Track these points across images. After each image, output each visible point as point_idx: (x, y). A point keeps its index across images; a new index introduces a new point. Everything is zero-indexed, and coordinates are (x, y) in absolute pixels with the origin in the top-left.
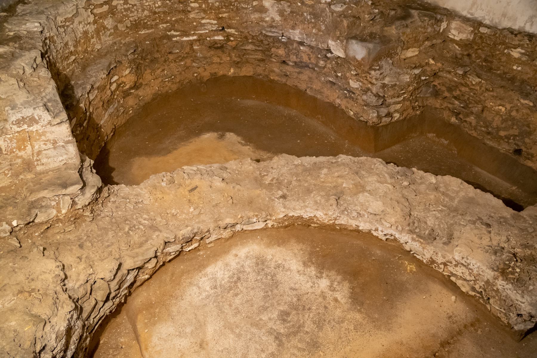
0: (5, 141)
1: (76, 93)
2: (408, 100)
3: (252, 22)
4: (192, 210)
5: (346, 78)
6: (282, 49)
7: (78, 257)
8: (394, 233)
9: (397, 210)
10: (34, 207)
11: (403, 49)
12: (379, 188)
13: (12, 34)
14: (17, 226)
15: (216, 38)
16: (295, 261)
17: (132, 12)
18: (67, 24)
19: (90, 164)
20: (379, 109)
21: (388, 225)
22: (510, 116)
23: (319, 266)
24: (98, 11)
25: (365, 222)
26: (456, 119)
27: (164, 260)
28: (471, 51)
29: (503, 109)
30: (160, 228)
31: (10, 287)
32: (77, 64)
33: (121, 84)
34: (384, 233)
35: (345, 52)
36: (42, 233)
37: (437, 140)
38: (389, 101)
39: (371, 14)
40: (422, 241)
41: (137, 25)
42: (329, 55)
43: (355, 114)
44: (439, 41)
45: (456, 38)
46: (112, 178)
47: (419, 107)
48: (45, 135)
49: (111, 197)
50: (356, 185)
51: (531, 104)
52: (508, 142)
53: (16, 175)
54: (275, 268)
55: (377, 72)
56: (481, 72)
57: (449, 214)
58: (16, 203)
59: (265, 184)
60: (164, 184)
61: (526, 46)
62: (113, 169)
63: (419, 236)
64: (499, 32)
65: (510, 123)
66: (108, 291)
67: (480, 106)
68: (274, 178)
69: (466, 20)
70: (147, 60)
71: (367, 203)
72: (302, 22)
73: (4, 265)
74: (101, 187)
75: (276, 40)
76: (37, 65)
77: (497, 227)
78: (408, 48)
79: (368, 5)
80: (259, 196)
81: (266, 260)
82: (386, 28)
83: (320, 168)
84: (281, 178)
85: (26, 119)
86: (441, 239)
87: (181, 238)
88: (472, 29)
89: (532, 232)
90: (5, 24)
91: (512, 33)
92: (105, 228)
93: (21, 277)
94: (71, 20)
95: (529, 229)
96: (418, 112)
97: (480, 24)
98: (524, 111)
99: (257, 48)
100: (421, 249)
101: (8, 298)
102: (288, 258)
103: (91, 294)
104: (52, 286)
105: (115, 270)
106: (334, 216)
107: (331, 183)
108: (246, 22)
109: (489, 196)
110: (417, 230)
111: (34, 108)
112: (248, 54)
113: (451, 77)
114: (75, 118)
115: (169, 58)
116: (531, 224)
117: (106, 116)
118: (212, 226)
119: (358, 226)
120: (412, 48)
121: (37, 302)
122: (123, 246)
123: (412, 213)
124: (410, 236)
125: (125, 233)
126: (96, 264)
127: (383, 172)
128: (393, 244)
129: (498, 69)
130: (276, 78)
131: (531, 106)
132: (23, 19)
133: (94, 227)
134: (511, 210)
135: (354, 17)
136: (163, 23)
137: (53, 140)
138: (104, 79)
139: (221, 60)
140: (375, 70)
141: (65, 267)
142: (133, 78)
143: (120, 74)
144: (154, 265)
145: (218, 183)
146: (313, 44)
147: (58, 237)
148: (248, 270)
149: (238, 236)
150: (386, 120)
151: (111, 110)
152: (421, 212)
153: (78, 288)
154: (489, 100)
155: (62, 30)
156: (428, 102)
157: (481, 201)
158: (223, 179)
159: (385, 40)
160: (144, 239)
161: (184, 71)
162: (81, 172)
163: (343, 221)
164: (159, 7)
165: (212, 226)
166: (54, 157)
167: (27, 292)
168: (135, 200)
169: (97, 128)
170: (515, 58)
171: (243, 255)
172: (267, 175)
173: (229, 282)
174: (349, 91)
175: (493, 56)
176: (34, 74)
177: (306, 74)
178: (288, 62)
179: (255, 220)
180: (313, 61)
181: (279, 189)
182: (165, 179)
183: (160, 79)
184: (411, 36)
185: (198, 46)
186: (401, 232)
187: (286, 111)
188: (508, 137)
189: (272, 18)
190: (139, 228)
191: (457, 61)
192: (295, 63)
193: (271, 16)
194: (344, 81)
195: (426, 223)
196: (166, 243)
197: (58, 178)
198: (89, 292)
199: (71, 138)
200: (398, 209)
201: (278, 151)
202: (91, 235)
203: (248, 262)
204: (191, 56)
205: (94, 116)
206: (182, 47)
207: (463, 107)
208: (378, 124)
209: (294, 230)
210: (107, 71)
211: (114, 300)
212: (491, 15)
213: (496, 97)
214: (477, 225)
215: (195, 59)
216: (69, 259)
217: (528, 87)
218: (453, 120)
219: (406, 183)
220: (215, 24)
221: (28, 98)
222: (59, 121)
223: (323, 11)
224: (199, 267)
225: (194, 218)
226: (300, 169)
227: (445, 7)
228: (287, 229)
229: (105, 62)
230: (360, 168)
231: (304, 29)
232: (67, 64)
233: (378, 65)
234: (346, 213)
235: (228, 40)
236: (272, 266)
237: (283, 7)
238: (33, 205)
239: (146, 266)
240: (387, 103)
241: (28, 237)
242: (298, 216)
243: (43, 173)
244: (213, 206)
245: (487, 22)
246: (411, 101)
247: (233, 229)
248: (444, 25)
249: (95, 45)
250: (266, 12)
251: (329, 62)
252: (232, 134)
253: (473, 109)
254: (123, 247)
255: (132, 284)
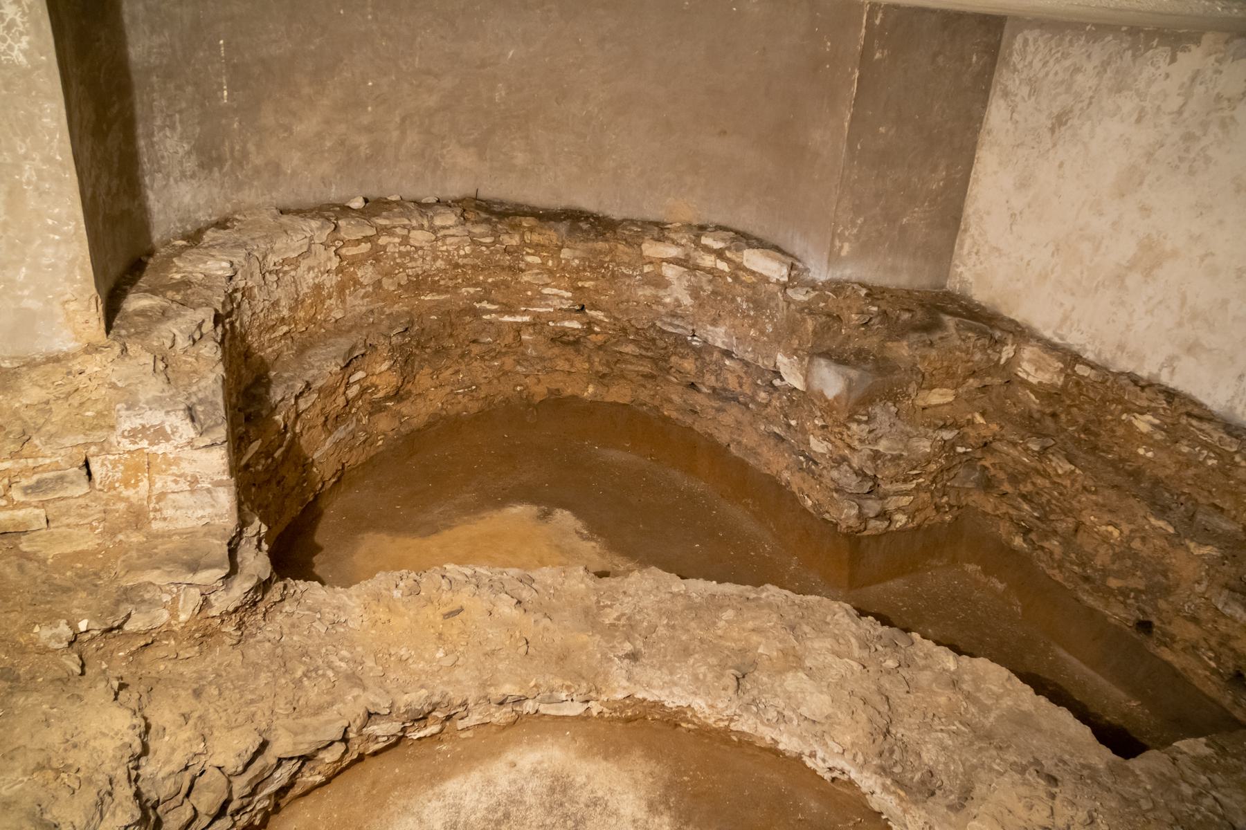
0: (103, 465)
1: (272, 393)
2: (927, 489)
3: (638, 303)
4: (440, 654)
5: (804, 432)
6: (691, 360)
7: (183, 715)
8: (847, 768)
9: (858, 719)
10: (127, 600)
11: (920, 388)
12: (831, 667)
13: (178, 276)
14: (87, 631)
15: (567, 324)
16: (631, 797)
17: (412, 259)
18: (286, 268)
19: (259, 533)
20: (862, 502)
21: (838, 749)
22: (1130, 548)
23: (680, 817)
24: (348, 251)
25: (792, 734)
26: (1025, 540)
27: (362, 749)
28: (1059, 409)
29: (1116, 533)
30: (366, 682)
31: (25, 754)
32: (289, 342)
33: (368, 388)
34: (827, 765)
35: (806, 380)
36: (132, 654)
37: (983, 579)
38: (886, 487)
39: (863, 313)
40: (902, 794)
41: (418, 284)
42: (777, 382)
43: (814, 505)
44: (998, 381)
45: (1031, 379)
46: (313, 565)
47: (951, 507)
48: (178, 465)
49: (286, 603)
50: (785, 653)
51: (1171, 530)
52: (1124, 603)
53: (112, 532)
54: (587, 806)
55: (863, 426)
56: (1076, 452)
57: (971, 744)
58: (96, 586)
59: (602, 623)
60: (397, 594)
61: (1161, 411)
62: (319, 549)
63: (898, 783)
64: (1111, 378)
65: (1129, 563)
66: (225, 796)
67: (1070, 520)
68: (623, 615)
69: (1050, 347)
70: (428, 350)
71: (799, 695)
72: (732, 313)
73: (34, 705)
74: (270, 579)
75: (680, 341)
76: (202, 336)
77: (1071, 786)
78: (931, 388)
79: (859, 296)
80: (583, 647)
81: (571, 785)
82: (889, 344)
83: (721, 608)
84: (638, 617)
85: (149, 429)
86: (947, 797)
87: (403, 710)
88: (1061, 365)
89: (1148, 811)
90: (175, 260)
91: (1136, 383)
92: (255, 665)
93: (54, 737)
94: (295, 262)
95: (1142, 802)
96: (948, 518)
97: (1077, 358)
98: (1157, 542)
99: (644, 353)
100: (898, 811)
101: (13, 776)
102: (619, 789)
103: (188, 795)
104: (107, 767)
105: (249, 754)
106: (728, 712)
107: (735, 641)
108: (628, 301)
109: (1064, 715)
110: (897, 769)
111: (167, 413)
112: (625, 362)
113: (1017, 453)
114: (260, 441)
115: (470, 351)
116: (1149, 792)
117: (328, 444)
118: (472, 696)
119: (777, 742)
120: (942, 386)
121: (65, 794)
122: (282, 706)
123: (893, 731)
124: (880, 781)
125: (294, 681)
126: (216, 734)
127: (847, 633)
128: (846, 791)
129: (1109, 450)
130: (674, 415)
131: (1170, 535)
132: (207, 254)
133: (236, 657)
134: (1107, 753)
135: (829, 315)
136: (469, 286)
137: (192, 476)
138: (336, 374)
139: (572, 366)
140: (859, 422)
141: (152, 731)
142: (394, 380)
143: (370, 370)
144: (337, 757)
145: (506, 608)
146: (749, 357)
147: (162, 667)
148: (530, 799)
149: (524, 724)
150: (879, 525)
151: (340, 433)
152: (911, 730)
153: (164, 779)
154: (1089, 511)
155: (271, 278)
156: (970, 499)
157: (1045, 724)
158: (519, 602)
159: (884, 366)
160: (328, 698)
161: (498, 379)
162: (237, 544)
163: (746, 724)
164: (466, 256)
165: (472, 696)
166: (188, 508)
167: (52, 769)
168: (331, 617)
169: (305, 465)
170: (1142, 433)
171: (528, 767)
172: (611, 606)
173: (485, 819)
174: (809, 459)
175: (1100, 423)
176: (191, 350)
177: (733, 413)
178: (700, 386)
179: (563, 696)
180: (747, 389)
181: (628, 638)
182: (402, 584)
183: (448, 389)
184: (938, 365)
185: (531, 335)
186: (863, 767)
187: (685, 482)
188: (1124, 592)
189: (677, 300)
190: (324, 675)
191: (1030, 424)
192: (714, 389)
193: (675, 295)
194: (800, 436)
195: (919, 755)
196: (370, 715)
197: (186, 550)
198: (184, 791)
199: (226, 477)
200: (862, 717)
201: (646, 561)
202: (224, 674)
203: (534, 783)
204: (515, 353)
205: (302, 442)
206: (499, 333)
207: (1038, 518)
208: (860, 531)
209: (642, 730)
210: (344, 360)
211: (237, 818)
212: (1097, 343)
213: (1104, 506)
214: (1027, 776)
215: (522, 359)
216: (162, 714)
217: (1167, 495)
218: (1018, 541)
219: (891, 663)
220: (568, 299)
221: (163, 391)
222: (209, 443)
223: (772, 297)
224: (433, 776)
225: (441, 673)
226: (680, 603)
227: (1012, 317)
228: (630, 725)
229: (344, 344)
230: (803, 617)
231: (733, 327)
232: (270, 340)
233: (868, 414)
234: (755, 709)
235: (590, 330)
236: (583, 799)
237: (700, 281)
238: (127, 595)
239: (321, 755)
240: (881, 491)
241: (102, 657)
242: (655, 702)
243: (163, 536)
244: (486, 654)
245: (1089, 356)
246: (932, 493)
247: (518, 709)
248: (1007, 352)
249: (331, 311)
250: (666, 287)
251: (776, 395)
252: (567, 513)
253: (1058, 525)
254: (282, 707)
255: (283, 791)
